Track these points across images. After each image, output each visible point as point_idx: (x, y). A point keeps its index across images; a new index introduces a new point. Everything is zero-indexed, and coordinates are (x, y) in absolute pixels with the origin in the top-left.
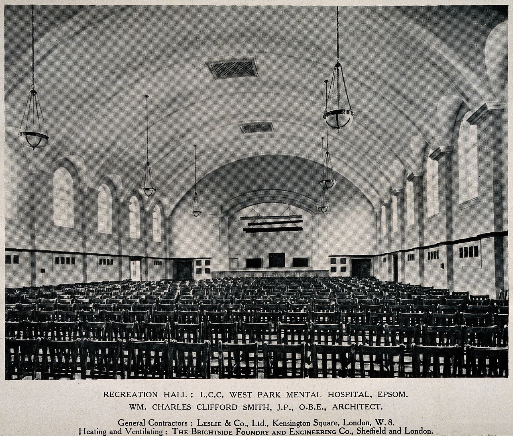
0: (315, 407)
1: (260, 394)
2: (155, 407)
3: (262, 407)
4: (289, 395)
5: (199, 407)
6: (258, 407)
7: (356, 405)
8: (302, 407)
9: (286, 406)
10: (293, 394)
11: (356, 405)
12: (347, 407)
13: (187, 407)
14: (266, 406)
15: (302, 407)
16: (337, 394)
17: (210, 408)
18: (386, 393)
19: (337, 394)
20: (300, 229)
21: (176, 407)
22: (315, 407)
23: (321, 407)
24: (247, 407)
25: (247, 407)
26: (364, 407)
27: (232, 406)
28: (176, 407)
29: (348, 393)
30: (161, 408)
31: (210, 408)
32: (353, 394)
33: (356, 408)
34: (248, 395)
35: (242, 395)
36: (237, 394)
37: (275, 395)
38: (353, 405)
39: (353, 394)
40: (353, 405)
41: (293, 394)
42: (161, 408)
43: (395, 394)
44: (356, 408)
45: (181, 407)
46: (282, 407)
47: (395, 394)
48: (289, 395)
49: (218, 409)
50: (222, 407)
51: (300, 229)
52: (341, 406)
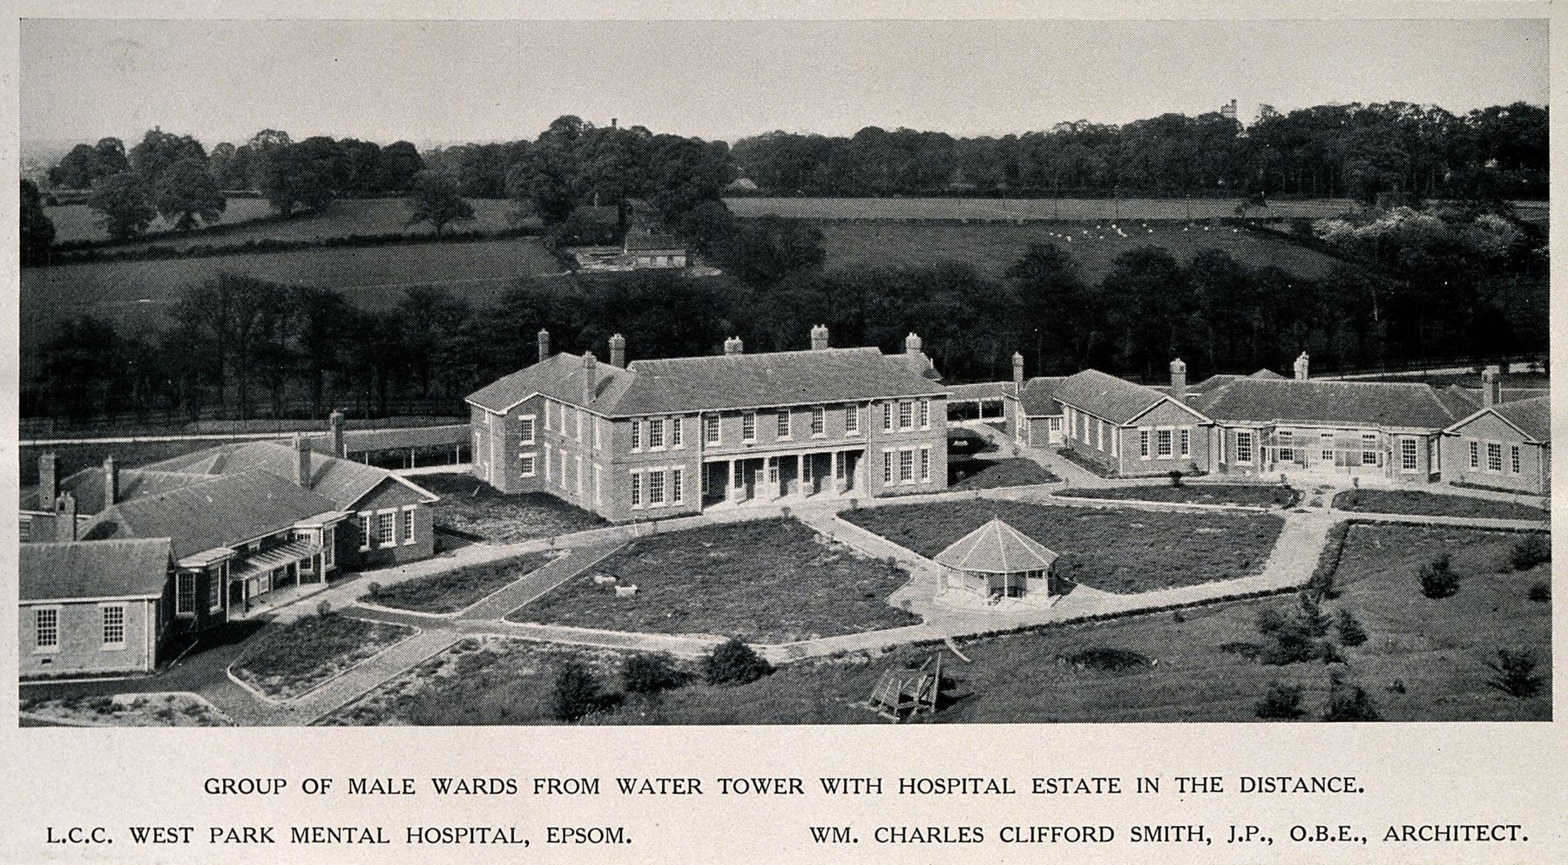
0: (1333, 832)
1: (217, 832)
2: (883, 835)
3: (1184, 834)
4: (1251, 785)
5: (1008, 835)
6: (1462, 833)
7: (1452, 831)
8: (1298, 833)
9: (1252, 830)
10: (311, 832)
11: (1452, 831)
12: (1427, 833)
13: (971, 835)
14: (1196, 829)
15: (1298, 833)
16: (433, 836)
17: (1036, 838)
18: (568, 832)
19: (433, 836)
20: (1474, 463)
21: (942, 836)
22: (1333, 832)
23: (1351, 834)
24: (1142, 832)
25: (1142, 832)
26: (1473, 833)
27: (1098, 831)
28: (942, 836)
29: (462, 832)
30: (898, 839)
31: (1036, 838)
32: (478, 835)
33: (1452, 836)
34: (181, 835)
35: (165, 836)
36: (152, 832)
37: (258, 836)
38: (1443, 829)
39: (478, 835)
40: (1443, 829)
41: (311, 832)
42: (898, 839)
43: (596, 836)
44: (1452, 836)
45: (954, 834)
46: (1241, 832)
47: (596, 836)
48: (1251, 785)
49: (1060, 839)
50: (1072, 834)
51: (1474, 463)
52: (1409, 830)
